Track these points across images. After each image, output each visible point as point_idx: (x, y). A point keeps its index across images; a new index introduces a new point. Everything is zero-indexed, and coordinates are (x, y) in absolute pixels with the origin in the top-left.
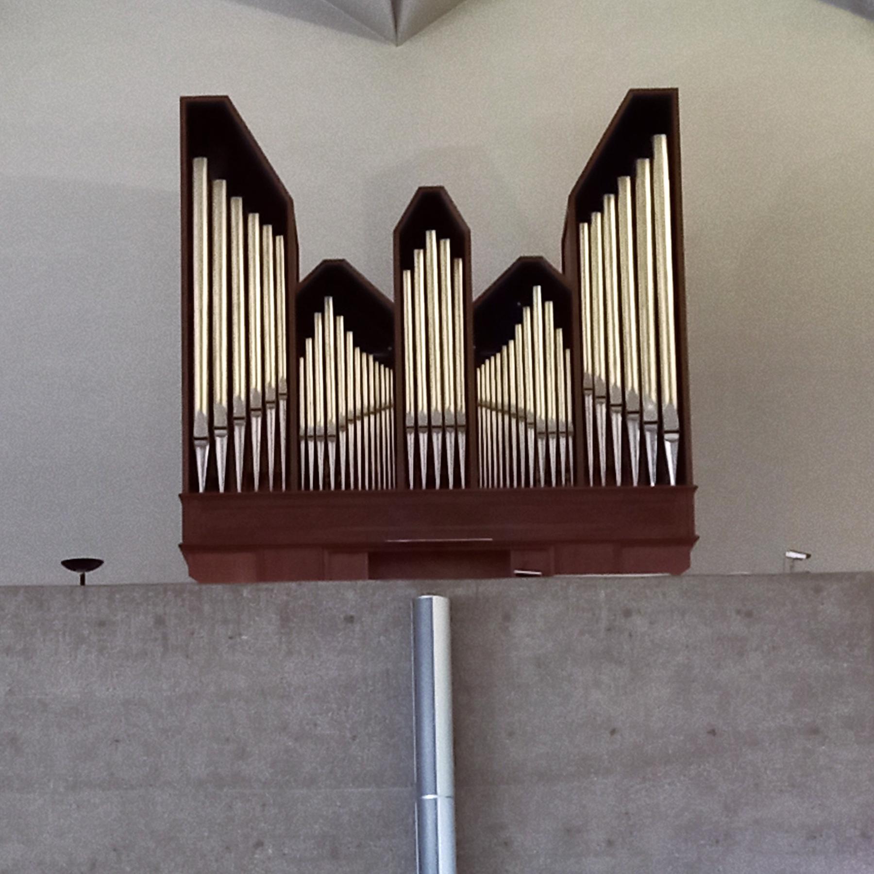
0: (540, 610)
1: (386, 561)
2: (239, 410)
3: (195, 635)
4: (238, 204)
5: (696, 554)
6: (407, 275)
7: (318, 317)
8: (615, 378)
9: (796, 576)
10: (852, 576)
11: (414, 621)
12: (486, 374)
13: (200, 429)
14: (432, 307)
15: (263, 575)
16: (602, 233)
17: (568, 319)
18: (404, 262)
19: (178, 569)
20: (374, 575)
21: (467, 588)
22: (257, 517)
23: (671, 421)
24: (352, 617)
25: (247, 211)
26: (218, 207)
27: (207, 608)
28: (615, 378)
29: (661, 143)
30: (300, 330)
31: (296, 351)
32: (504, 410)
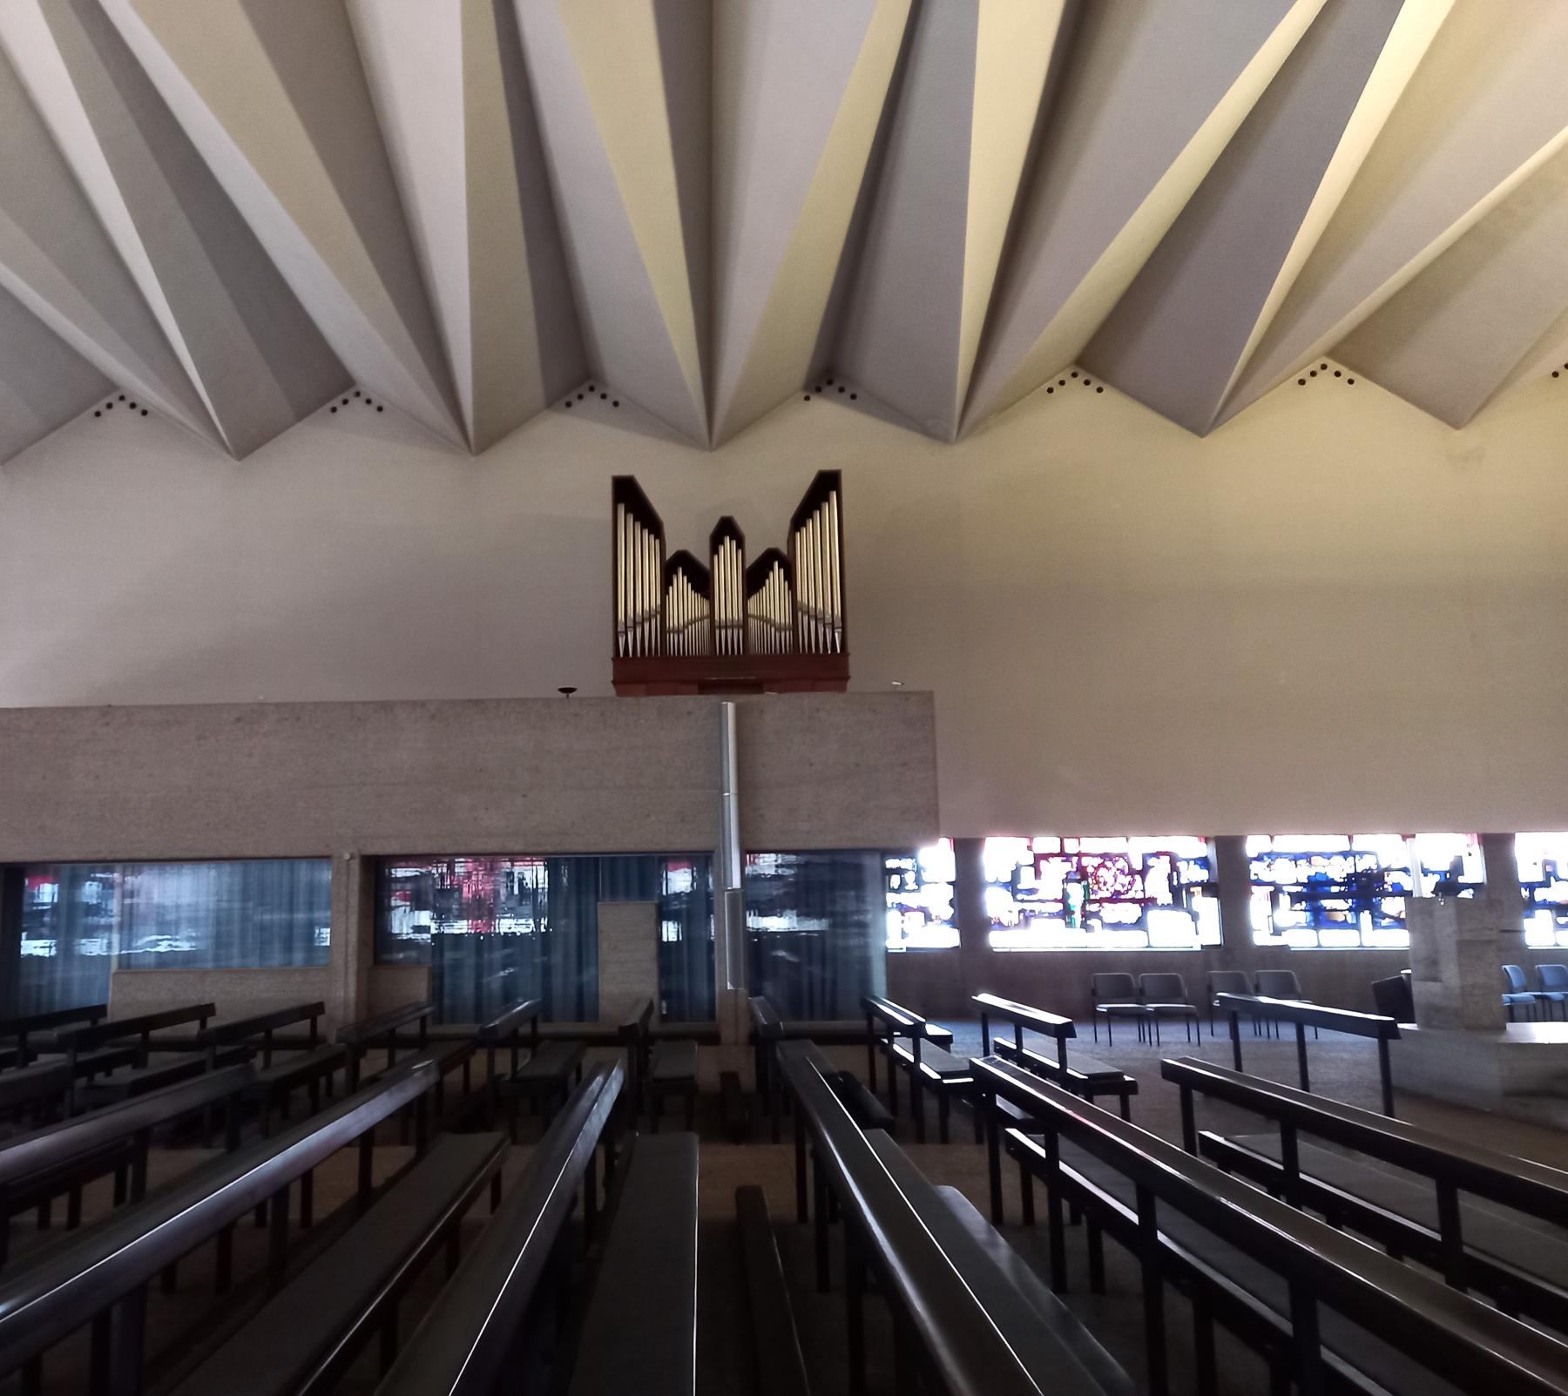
0: (776, 707)
1: (705, 688)
2: (639, 619)
4: (638, 525)
5: (850, 684)
8: (812, 604)
9: (895, 692)
11: (720, 713)
12: (752, 602)
13: (621, 628)
14: (727, 570)
15: (649, 693)
16: (806, 537)
17: (790, 577)
18: (714, 551)
19: (611, 691)
20: (700, 693)
21: (744, 698)
22: (648, 668)
23: (838, 623)
25: (642, 528)
26: (628, 526)
28: (812, 604)
30: (666, 583)
31: (665, 592)
32: (760, 618)
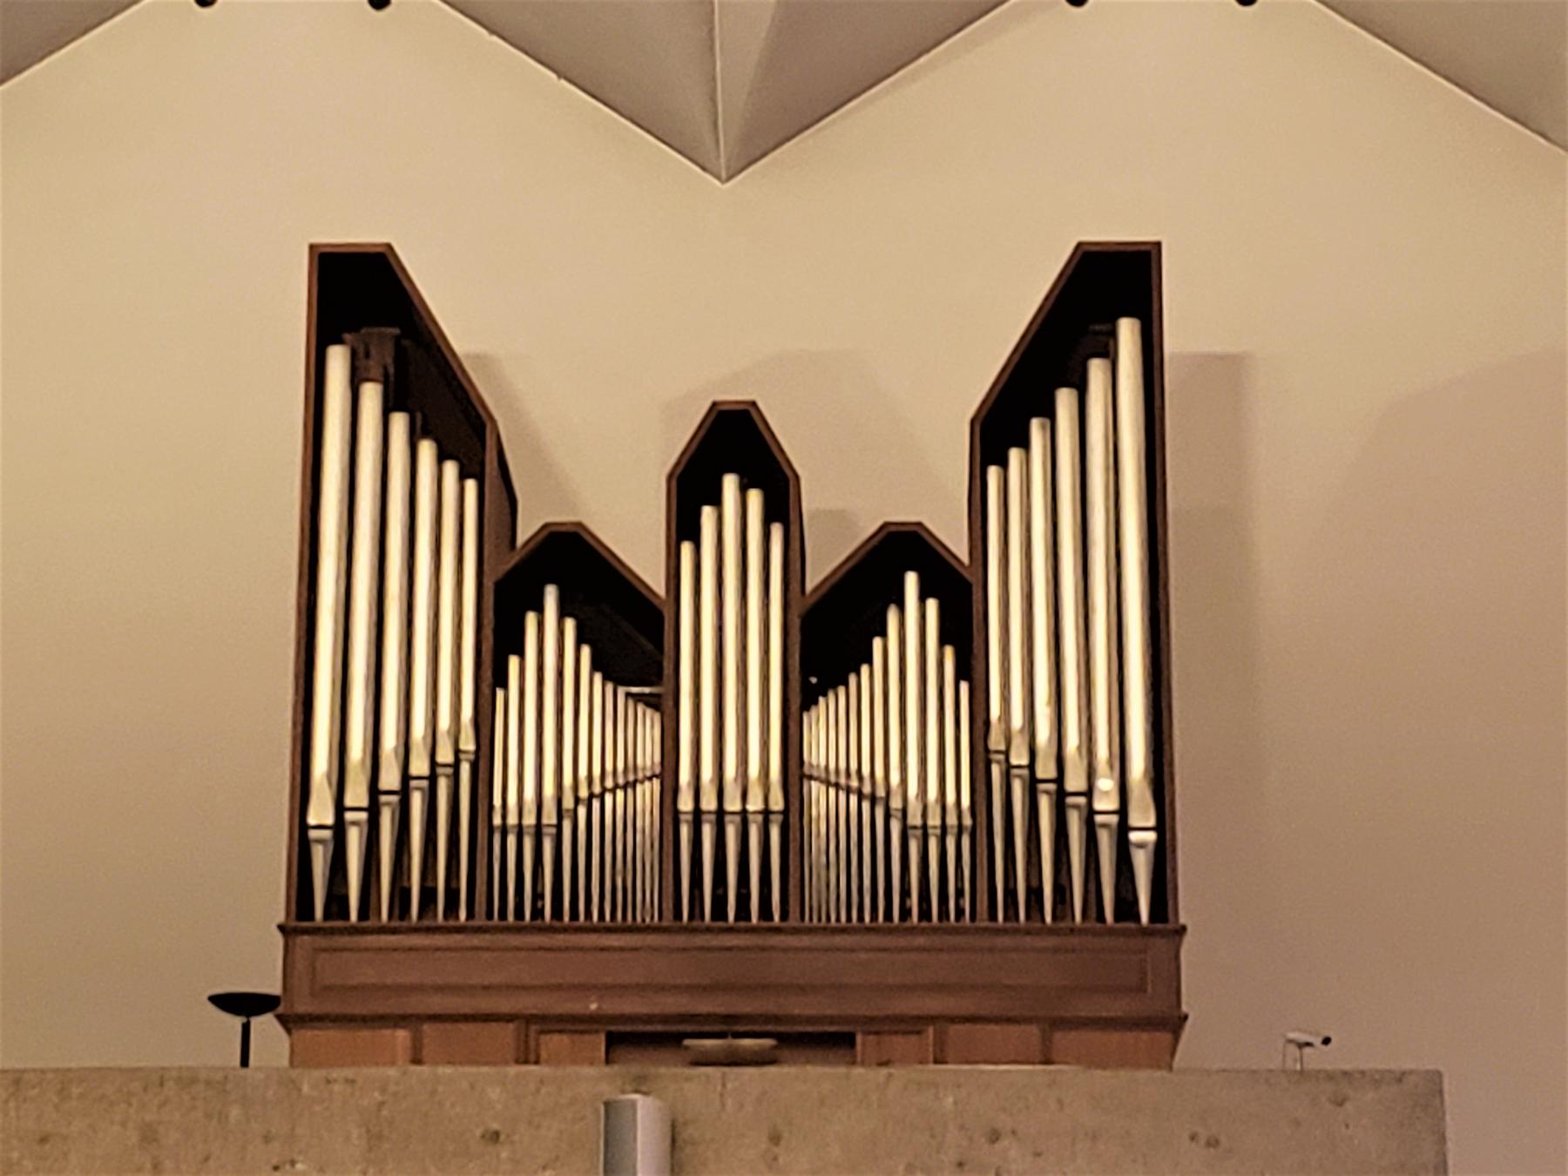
3: (211, 1162)
6: (686, 549)
7: (531, 619)
10: (1400, 1077)
12: (822, 739)
14: (732, 616)
16: (1026, 468)
17: (962, 631)
18: (684, 527)
24: (497, 1134)
27: (235, 1112)
29: (1128, 331)
30: (501, 640)
31: (492, 676)
